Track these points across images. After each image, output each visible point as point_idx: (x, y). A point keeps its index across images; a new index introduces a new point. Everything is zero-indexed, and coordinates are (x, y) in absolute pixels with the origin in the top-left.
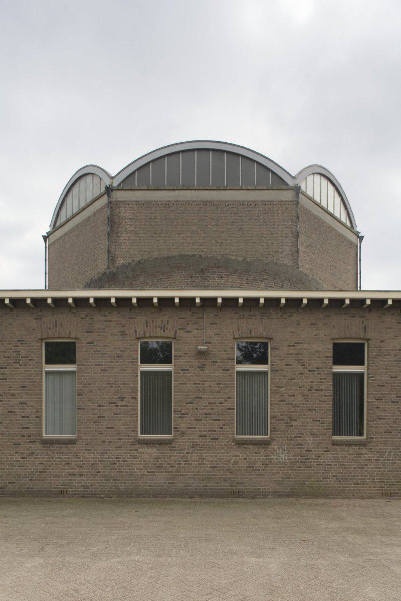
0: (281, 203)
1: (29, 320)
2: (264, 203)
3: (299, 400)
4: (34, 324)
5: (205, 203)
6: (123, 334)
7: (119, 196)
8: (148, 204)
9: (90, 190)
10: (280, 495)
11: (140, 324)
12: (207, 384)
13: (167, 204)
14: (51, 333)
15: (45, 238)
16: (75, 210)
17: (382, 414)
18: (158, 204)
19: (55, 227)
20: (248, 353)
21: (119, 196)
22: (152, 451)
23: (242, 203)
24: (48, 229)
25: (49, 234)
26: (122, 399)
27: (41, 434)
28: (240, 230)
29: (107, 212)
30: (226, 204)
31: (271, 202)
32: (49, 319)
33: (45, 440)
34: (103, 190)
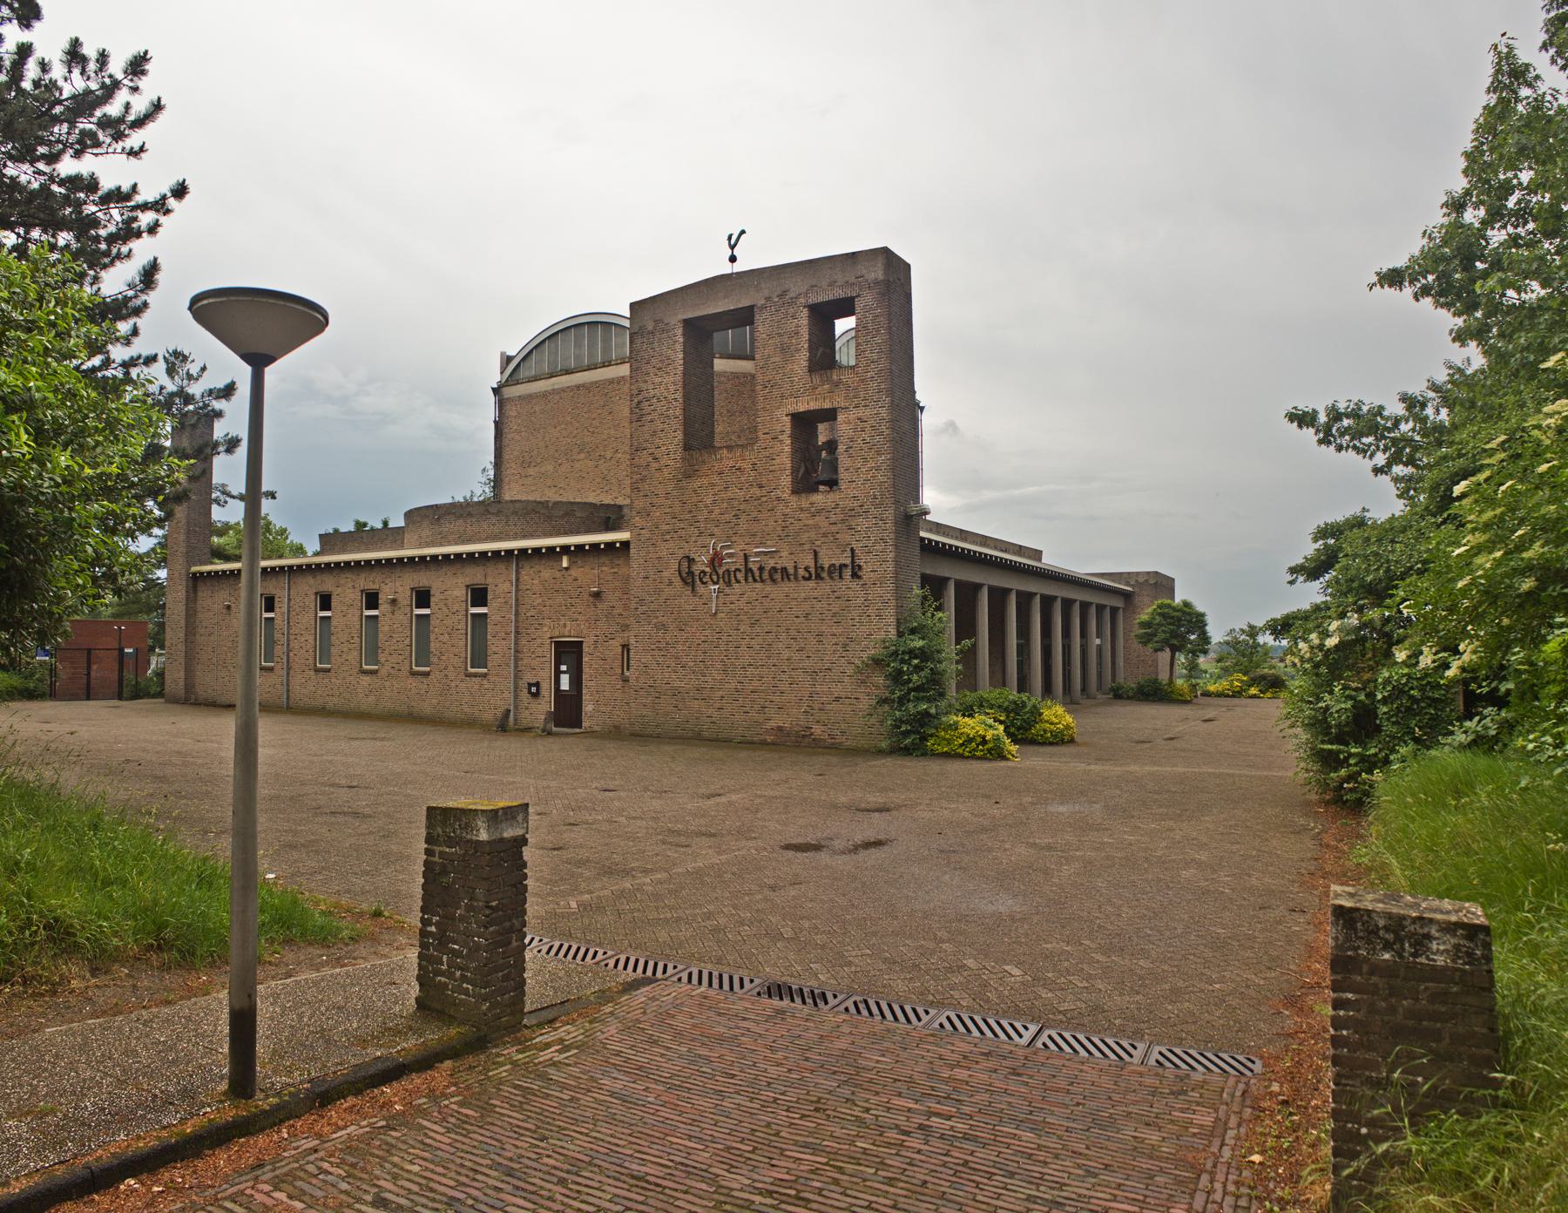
7: (510, 392)
13: (544, 395)
22: (366, 679)
23: (611, 381)
30: (596, 384)
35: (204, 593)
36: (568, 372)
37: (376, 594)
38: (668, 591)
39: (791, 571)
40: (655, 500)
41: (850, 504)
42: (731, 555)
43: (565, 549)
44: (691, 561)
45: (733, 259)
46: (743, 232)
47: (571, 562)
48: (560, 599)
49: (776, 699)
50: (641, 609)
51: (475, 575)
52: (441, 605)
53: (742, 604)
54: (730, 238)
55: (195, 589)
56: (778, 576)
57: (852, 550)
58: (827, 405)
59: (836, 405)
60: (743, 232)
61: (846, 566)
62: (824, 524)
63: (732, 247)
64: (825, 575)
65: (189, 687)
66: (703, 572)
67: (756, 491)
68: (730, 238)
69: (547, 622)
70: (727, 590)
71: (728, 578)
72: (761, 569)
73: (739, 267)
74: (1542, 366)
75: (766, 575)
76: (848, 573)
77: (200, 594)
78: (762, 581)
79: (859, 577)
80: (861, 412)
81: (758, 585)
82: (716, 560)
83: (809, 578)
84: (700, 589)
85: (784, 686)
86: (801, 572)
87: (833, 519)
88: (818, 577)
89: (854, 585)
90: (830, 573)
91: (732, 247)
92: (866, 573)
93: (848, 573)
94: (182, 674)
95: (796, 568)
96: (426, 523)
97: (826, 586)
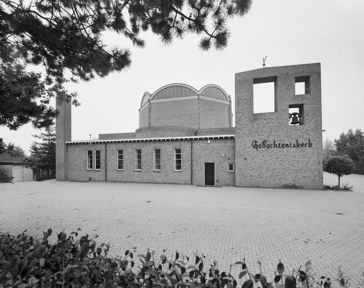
0: (195, 99)
1: (114, 145)
2: (190, 100)
3: (166, 162)
4: (115, 146)
5: (174, 101)
6: (132, 148)
7: (152, 101)
8: (159, 103)
9: (147, 98)
10: (163, 183)
11: (135, 146)
12: (148, 158)
13: (164, 103)
14: (118, 148)
15: (139, 110)
16: (145, 103)
17: (185, 165)
18: (161, 103)
19: (142, 107)
20: (9, 179)
21: (152, 101)
22: (137, 173)
23: (184, 100)
24: (140, 107)
25: (140, 109)
26: (131, 162)
27: (117, 169)
28: (183, 108)
29: (149, 106)
30: (179, 101)
31: (192, 99)
32: (118, 145)
33: (24, 155)
34: (147, 101)
35: (70, 148)
36: (169, 97)
37: (140, 150)
38: (248, 150)
39: (289, 145)
40: (243, 126)
41: (307, 128)
42: (269, 141)
43: (211, 139)
44: (256, 142)
45: (264, 65)
46: (267, 56)
47: (211, 142)
48: (207, 151)
49: (284, 177)
50: (239, 154)
51: (177, 145)
52: (165, 153)
53: (273, 153)
54: (263, 59)
55: (67, 148)
56: (285, 146)
57: (309, 140)
58: (301, 103)
59: (303, 103)
60: (267, 56)
61: (307, 144)
62: (300, 134)
63: (264, 62)
64: (300, 146)
65: (66, 176)
66: (261, 145)
67: (278, 125)
68: (263, 59)
69: (203, 158)
70: (268, 150)
71: (269, 146)
72: (279, 144)
73: (265, 67)
74: (65, 240)
75: (281, 146)
76: (307, 145)
77: (69, 149)
78: (279, 147)
79: (311, 147)
80: (313, 106)
81: (278, 148)
82: (264, 142)
83: (295, 147)
84: (259, 149)
85: (287, 174)
86: (292, 145)
87: (302, 132)
88: (298, 146)
89: (310, 148)
90: (301, 146)
91: (264, 62)
92: (313, 146)
93: (307, 145)
94: (64, 173)
95: (290, 144)
96: (149, 131)
97: (300, 149)
